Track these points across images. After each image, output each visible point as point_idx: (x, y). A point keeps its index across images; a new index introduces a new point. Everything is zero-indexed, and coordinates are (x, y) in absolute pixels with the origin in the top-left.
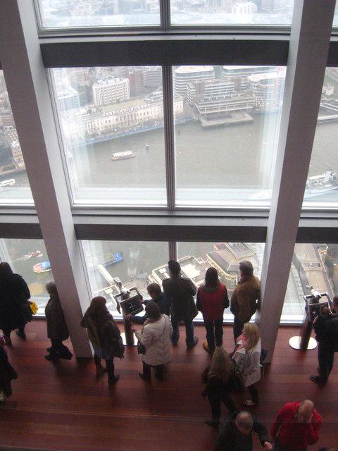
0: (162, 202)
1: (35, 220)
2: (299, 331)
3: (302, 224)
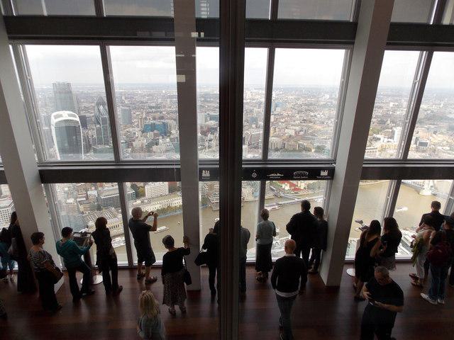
2: (352, 266)
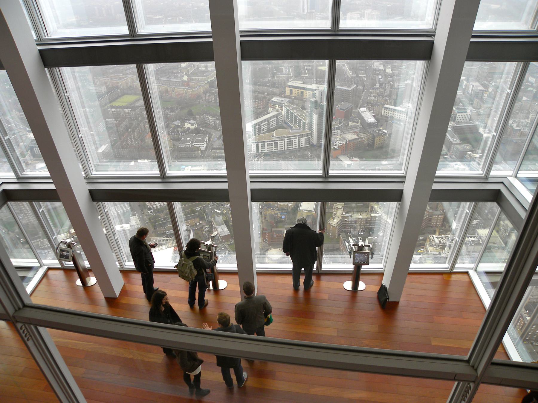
0: (320, 172)
1: (225, 186)
2: (351, 277)
3: (435, 187)
